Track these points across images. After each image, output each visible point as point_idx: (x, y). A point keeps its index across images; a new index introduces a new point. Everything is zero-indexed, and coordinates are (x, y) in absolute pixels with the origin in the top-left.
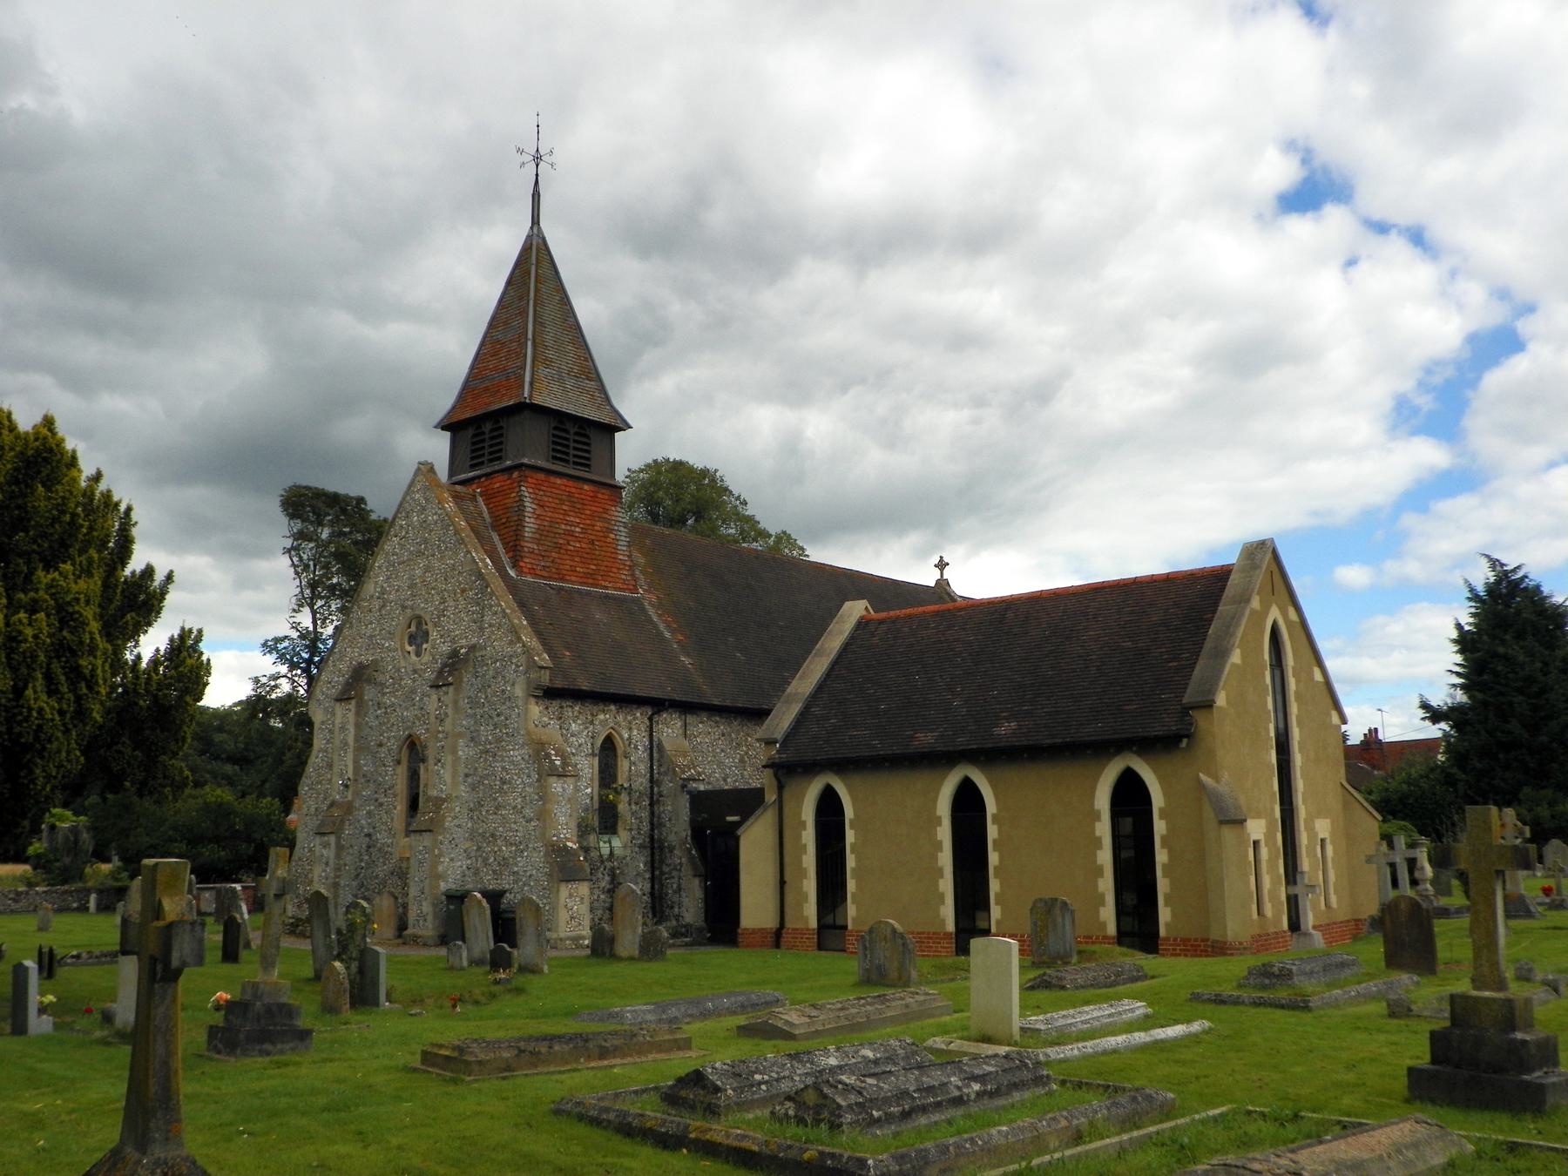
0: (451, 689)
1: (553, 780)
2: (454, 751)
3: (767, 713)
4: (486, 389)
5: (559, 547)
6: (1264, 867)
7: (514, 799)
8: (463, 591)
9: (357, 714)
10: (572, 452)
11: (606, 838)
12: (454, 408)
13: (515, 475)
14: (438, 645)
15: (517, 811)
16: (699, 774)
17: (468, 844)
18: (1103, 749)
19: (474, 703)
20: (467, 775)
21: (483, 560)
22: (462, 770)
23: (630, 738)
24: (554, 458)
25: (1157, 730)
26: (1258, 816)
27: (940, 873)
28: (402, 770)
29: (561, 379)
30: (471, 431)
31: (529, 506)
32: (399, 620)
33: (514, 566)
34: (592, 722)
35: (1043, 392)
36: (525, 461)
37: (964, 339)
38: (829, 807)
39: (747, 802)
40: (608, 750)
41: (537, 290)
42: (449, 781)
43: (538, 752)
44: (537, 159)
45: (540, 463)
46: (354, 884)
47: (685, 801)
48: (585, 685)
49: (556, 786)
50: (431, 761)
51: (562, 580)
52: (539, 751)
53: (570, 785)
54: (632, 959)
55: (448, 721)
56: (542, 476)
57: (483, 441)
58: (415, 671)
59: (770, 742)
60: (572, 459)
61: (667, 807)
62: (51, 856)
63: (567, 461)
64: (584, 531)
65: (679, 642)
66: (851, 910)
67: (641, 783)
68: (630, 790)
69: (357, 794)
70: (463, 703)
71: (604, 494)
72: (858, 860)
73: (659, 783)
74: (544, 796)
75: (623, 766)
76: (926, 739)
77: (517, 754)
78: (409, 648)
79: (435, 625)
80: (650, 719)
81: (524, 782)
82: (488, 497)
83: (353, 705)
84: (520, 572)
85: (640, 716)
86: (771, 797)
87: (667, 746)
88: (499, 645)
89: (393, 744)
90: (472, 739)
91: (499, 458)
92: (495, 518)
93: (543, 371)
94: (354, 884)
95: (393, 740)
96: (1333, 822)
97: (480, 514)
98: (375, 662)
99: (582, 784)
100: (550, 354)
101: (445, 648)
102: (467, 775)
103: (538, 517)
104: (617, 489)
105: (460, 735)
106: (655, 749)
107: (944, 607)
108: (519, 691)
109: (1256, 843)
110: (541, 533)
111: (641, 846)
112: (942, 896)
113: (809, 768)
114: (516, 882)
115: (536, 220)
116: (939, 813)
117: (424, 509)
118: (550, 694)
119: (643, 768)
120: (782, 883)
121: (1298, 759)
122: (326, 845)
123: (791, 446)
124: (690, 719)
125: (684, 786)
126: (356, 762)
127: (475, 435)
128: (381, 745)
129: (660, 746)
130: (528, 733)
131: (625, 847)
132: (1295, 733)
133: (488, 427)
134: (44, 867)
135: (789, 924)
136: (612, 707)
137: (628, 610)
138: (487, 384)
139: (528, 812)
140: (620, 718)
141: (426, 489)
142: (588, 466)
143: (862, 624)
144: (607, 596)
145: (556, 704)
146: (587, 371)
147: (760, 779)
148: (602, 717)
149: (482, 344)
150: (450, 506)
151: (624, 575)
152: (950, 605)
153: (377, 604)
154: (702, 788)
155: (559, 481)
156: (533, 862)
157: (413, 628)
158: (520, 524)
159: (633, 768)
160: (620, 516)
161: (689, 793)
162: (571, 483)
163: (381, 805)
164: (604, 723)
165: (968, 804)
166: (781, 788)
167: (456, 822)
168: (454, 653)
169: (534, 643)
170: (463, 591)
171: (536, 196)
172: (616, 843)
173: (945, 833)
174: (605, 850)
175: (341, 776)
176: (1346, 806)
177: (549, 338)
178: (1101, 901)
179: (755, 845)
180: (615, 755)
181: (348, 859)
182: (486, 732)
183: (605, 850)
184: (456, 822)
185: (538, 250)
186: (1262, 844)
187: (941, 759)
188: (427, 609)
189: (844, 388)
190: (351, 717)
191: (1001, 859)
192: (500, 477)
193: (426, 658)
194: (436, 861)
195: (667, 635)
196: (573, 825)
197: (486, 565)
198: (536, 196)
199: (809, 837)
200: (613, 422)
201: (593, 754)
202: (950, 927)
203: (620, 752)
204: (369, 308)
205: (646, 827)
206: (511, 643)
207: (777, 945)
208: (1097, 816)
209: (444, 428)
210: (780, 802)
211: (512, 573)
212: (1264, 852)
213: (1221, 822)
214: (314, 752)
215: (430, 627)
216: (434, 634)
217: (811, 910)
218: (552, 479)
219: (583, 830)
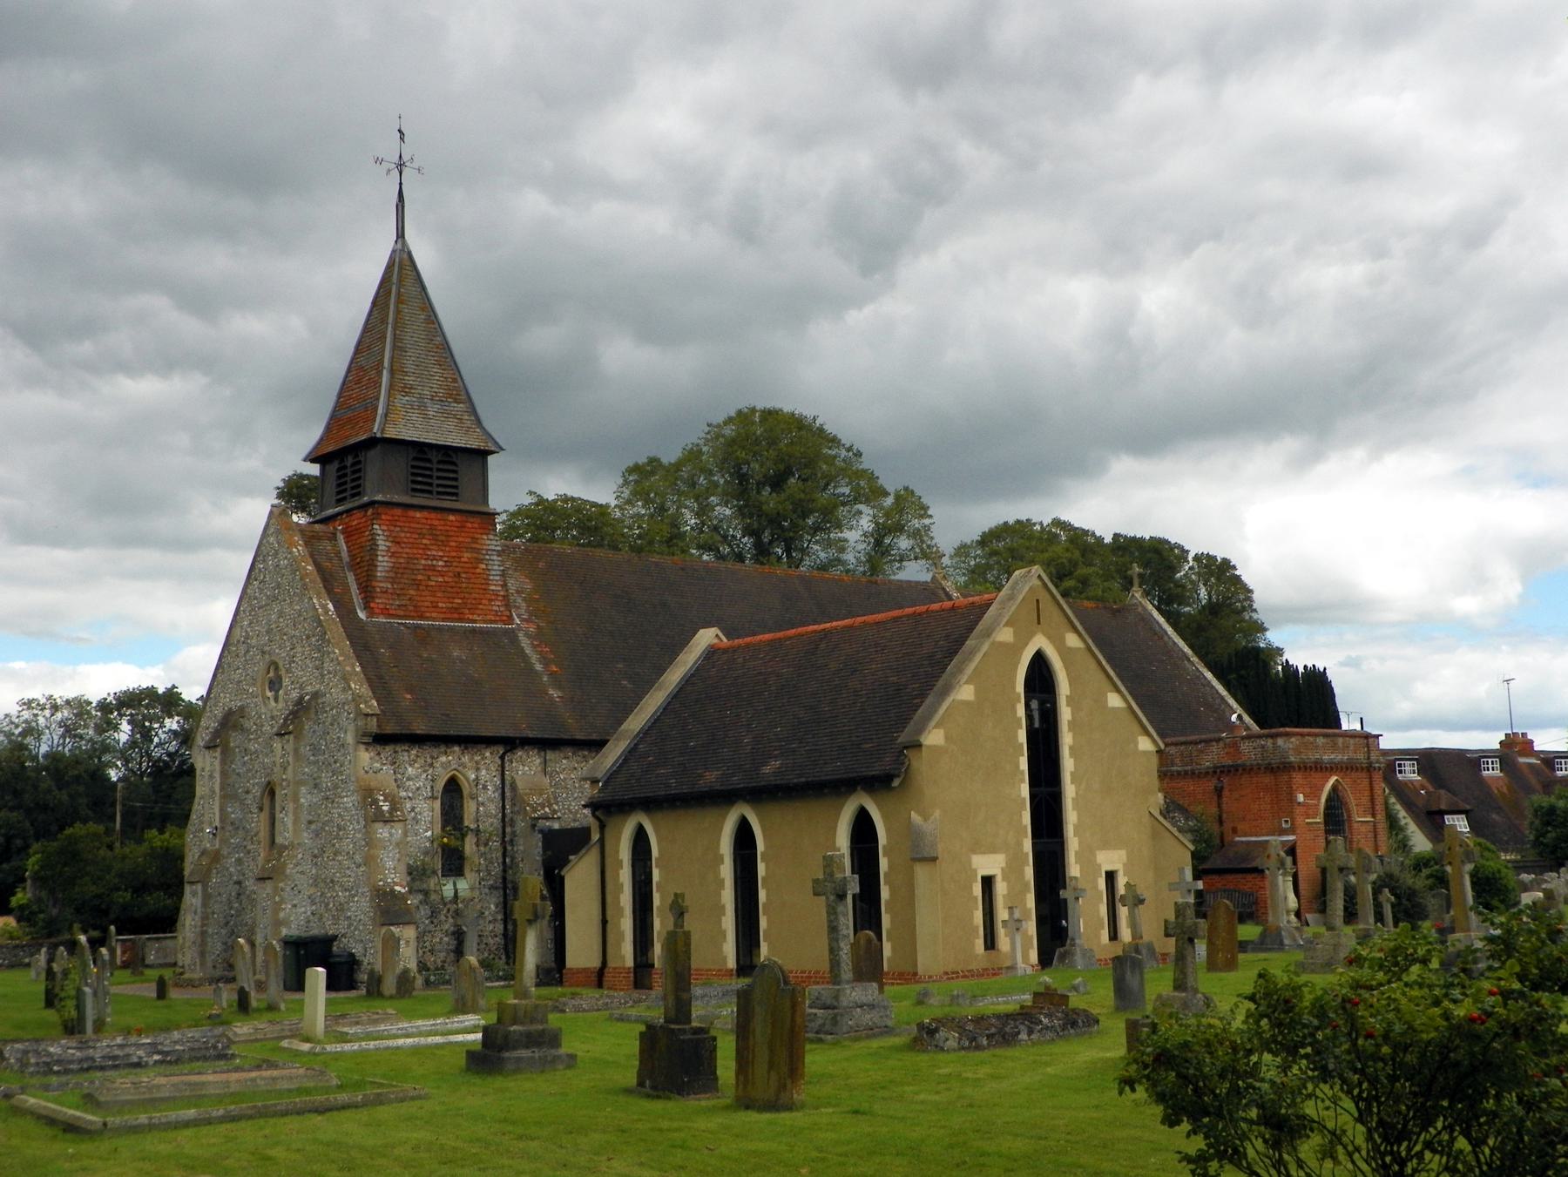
1: (379, 825)
2: (296, 799)
4: (350, 420)
5: (417, 584)
7: (346, 845)
8: (308, 637)
9: (223, 762)
11: (451, 880)
12: (321, 439)
13: (370, 512)
15: (350, 857)
16: (555, 812)
17: (312, 890)
19: (315, 750)
20: (310, 822)
21: (324, 607)
22: (304, 817)
24: (414, 490)
25: (876, 770)
26: (992, 850)
29: (422, 407)
30: (336, 465)
31: (382, 544)
33: (367, 607)
34: (431, 765)
35: (1474, 232)
36: (379, 498)
37: (1363, 165)
40: (453, 789)
41: (398, 312)
43: (365, 798)
45: (397, 498)
46: (224, 931)
47: (537, 841)
48: (420, 728)
49: (382, 832)
51: (421, 617)
52: (368, 795)
53: (398, 830)
54: (391, 997)
55: (290, 769)
56: (398, 511)
57: (345, 475)
59: (595, 782)
62: (35, 908)
63: (430, 492)
64: (448, 564)
65: (552, 674)
67: (491, 824)
68: (477, 832)
69: (224, 841)
70: (305, 750)
71: (473, 523)
74: (370, 842)
75: (470, 808)
76: (711, 778)
77: (349, 800)
78: (269, 694)
80: (502, 758)
81: (355, 827)
82: (348, 534)
83: (218, 753)
85: (490, 756)
86: (595, 837)
87: (520, 784)
88: (335, 694)
90: (316, 786)
91: (358, 494)
92: (353, 557)
93: (401, 400)
94: (224, 931)
97: (338, 554)
98: (242, 708)
99: (421, 828)
100: (410, 380)
101: (295, 695)
102: (310, 822)
103: (393, 555)
104: (491, 516)
105: (300, 783)
106: (506, 789)
107: (935, 606)
108: (350, 739)
110: (397, 572)
111: (491, 887)
112: (724, 934)
115: (401, 234)
118: (380, 740)
119: (493, 808)
120: (604, 922)
123: (1117, 334)
124: (550, 755)
125: (534, 826)
126: (222, 810)
127: (339, 470)
129: (514, 787)
130: (357, 780)
131: (472, 889)
133: (350, 460)
134: (28, 920)
135: (611, 964)
136: (456, 748)
137: (499, 643)
138: (350, 414)
140: (466, 759)
141: (278, 532)
142: (456, 494)
143: (711, 653)
144: (474, 630)
145: (389, 749)
146: (457, 393)
147: (586, 817)
148: (443, 759)
149: (349, 370)
150: (299, 549)
151: (497, 605)
153: (242, 649)
154: (556, 826)
155: (418, 515)
156: (361, 908)
157: (271, 674)
158: (372, 565)
159: (481, 808)
160: (492, 543)
161: (541, 831)
162: (433, 515)
166: (602, 827)
167: (299, 869)
168: (300, 700)
169: (365, 690)
170: (308, 637)
172: (463, 885)
174: (448, 890)
175: (210, 824)
176: (1155, 836)
177: (410, 366)
180: (462, 797)
182: (326, 779)
183: (448, 890)
184: (299, 870)
185: (401, 268)
186: (999, 879)
187: (723, 798)
188: (281, 655)
189: (1188, 246)
190: (217, 763)
191: (768, 896)
192: (358, 514)
193: (281, 705)
194: (277, 907)
195: (538, 667)
196: (403, 868)
197: (326, 611)
199: (625, 876)
200: (482, 446)
201: (433, 798)
202: (630, 963)
203: (466, 792)
204: (571, 183)
205: (496, 869)
206: (344, 690)
207: (600, 985)
210: (602, 841)
211: (362, 615)
212: (1001, 888)
213: (915, 860)
215: (282, 672)
216: (286, 681)
218: (411, 513)
219: (416, 874)
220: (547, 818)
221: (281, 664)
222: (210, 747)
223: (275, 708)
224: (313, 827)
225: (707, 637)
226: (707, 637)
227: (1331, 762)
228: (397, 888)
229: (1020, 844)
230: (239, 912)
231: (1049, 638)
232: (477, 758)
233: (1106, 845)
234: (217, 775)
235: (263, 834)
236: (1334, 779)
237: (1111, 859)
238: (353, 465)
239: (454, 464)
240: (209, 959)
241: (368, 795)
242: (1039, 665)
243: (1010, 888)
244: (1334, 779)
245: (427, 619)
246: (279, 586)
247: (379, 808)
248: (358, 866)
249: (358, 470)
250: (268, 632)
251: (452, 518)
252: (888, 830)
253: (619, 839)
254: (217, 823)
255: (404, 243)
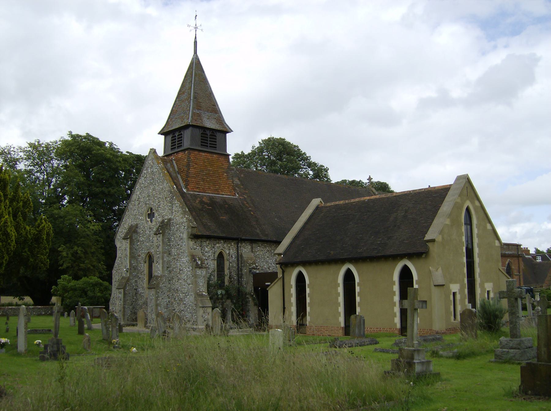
0: (161, 235)
3: (280, 242)
6: (458, 302)
7: (184, 276)
8: (166, 198)
10: (209, 142)
14: (158, 218)
18: (343, 261)
23: (229, 253)
24: (202, 145)
26: (456, 282)
27: (339, 304)
28: (146, 265)
30: (171, 136)
32: (144, 209)
34: (214, 247)
38: (300, 279)
39: (272, 277)
40: (221, 256)
42: (161, 269)
44: (196, 28)
46: (131, 307)
49: (199, 272)
50: (155, 262)
55: (160, 247)
56: (196, 153)
58: (150, 228)
60: (209, 145)
61: (245, 279)
63: (207, 146)
66: (308, 318)
69: (131, 273)
72: (311, 300)
73: (241, 270)
78: (149, 220)
79: (157, 211)
84: (188, 190)
86: (280, 275)
89: (143, 256)
92: (179, 169)
94: (131, 307)
95: (142, 255)
96: (494, 285)
98: (137, 225)
101: (160, 220)
102: (168, 268)
106: (239, 257)
108: (185, 236)
109: (454, 294)
113: (294, 264)
114: (185, 307)
116: (339, 282)
117: (152, 166)
120: (284, 308)
121: (477, 260)
122: (120, 293)
124: (254, 245)
125: (250, 271)
126: (130, 262)
127: (172, 137)
128: (139, 256)
129: (241, 256)
132: (476, 250)
136: (222, 241)
139: (189, 281)
140: (225, 245)
142: (216, 147)
143: (317, 208)
145: (199, 241)
148: (218, 245)
152: (389, 195)
153: (137, 203)
154: (258, 272)
155: (203, 154)
162: (208, 155)
163: (140, 278)
164: (218, 248)
165: (349, 277)
166: (283, 272)
170: (166, 198)
171: (195, 43)
173: (341, 290)
178: (395, 315)
179: (274, 292)
180: (224, 260)
181: (128, 298)
186: (458, 293)
188: (154, 205)
190: (128, 245)
191: (360, 299)
193: (154, 223)
198: (195, 43)
199: (293, 291)
201: (214, 259)
203: (225, 258)
208: (394, 283)
209: (162, 134)
210: (283, 277)
212: (458, 297)
214: (117, 258)
216: (156, 215)
217: (294, 318)
218: (201, 153)
220: (255, 269)
221: (154, 208)
222: (125, 238)
223: (154, 224)
224: (169, 269)
225: (316, 202)
226: (316, 202)
227: (508, 254)
228: (204, 293)
229: (464, 280)
230: (137, 300)
231: (471, 201)
232: (229, 245)
233: (487, 281)
234: (128, 249)
235: (146, 271)
236: (508, 260)
237: (489, 286)
238: (178, 135)
239: (215, 136)
240: (126, 317)
241: (193, 258)
242: (468, 210)
243: (461, 297)
244: (508, 260)
245: (207, 193)
246: (153, 179)
247: (197, 263)
248: (189, 285)
249: (181, 137)
250: (149, 196)
251: (215, 156)
252: (418, 275)
253: (291, 275)
254: (128, 267)
255: (197, 56)
